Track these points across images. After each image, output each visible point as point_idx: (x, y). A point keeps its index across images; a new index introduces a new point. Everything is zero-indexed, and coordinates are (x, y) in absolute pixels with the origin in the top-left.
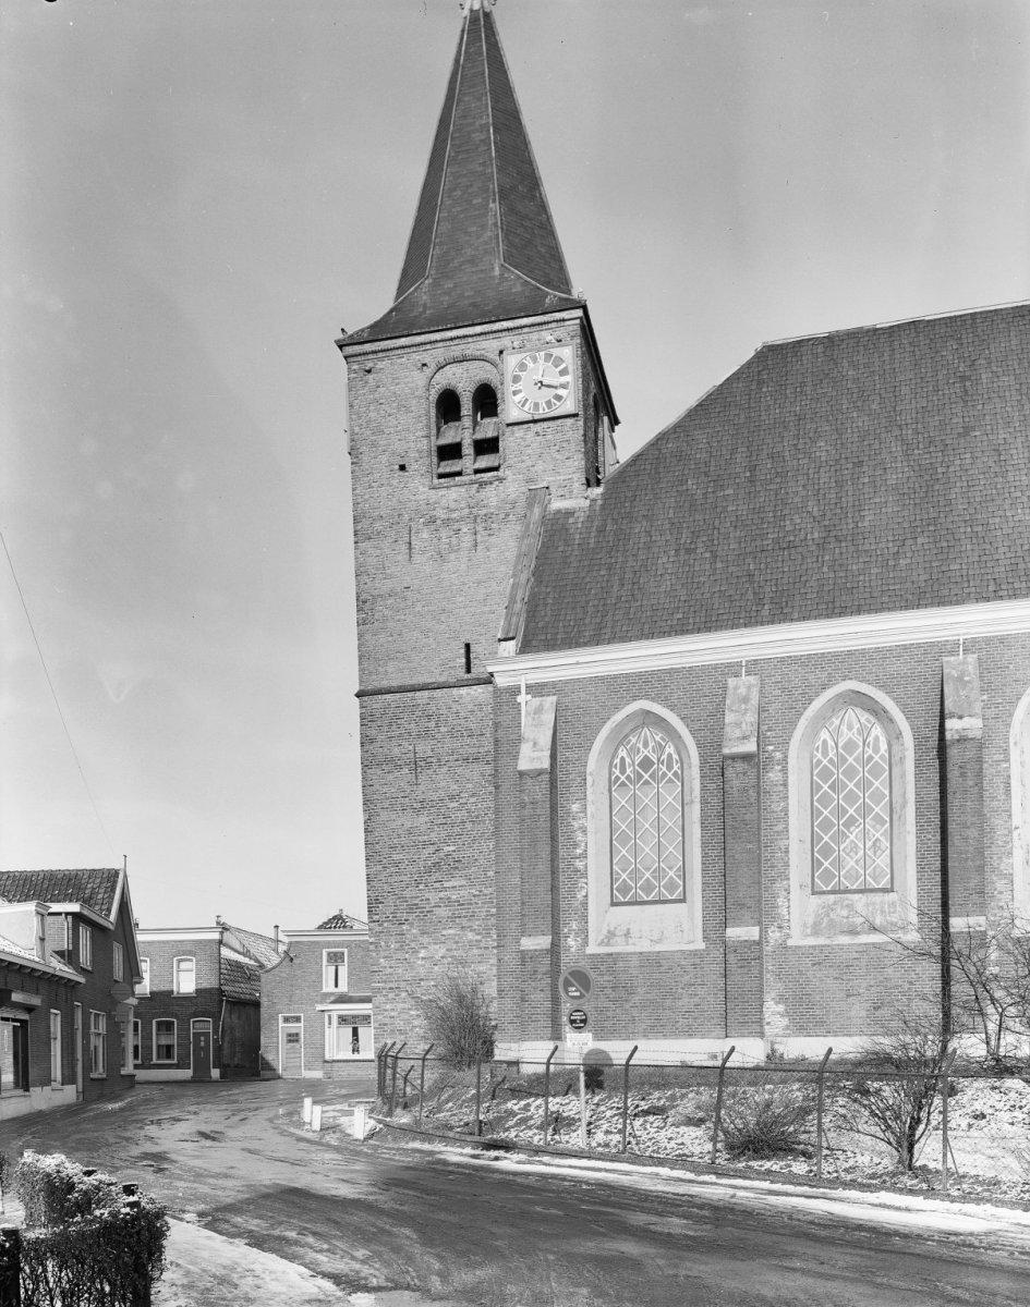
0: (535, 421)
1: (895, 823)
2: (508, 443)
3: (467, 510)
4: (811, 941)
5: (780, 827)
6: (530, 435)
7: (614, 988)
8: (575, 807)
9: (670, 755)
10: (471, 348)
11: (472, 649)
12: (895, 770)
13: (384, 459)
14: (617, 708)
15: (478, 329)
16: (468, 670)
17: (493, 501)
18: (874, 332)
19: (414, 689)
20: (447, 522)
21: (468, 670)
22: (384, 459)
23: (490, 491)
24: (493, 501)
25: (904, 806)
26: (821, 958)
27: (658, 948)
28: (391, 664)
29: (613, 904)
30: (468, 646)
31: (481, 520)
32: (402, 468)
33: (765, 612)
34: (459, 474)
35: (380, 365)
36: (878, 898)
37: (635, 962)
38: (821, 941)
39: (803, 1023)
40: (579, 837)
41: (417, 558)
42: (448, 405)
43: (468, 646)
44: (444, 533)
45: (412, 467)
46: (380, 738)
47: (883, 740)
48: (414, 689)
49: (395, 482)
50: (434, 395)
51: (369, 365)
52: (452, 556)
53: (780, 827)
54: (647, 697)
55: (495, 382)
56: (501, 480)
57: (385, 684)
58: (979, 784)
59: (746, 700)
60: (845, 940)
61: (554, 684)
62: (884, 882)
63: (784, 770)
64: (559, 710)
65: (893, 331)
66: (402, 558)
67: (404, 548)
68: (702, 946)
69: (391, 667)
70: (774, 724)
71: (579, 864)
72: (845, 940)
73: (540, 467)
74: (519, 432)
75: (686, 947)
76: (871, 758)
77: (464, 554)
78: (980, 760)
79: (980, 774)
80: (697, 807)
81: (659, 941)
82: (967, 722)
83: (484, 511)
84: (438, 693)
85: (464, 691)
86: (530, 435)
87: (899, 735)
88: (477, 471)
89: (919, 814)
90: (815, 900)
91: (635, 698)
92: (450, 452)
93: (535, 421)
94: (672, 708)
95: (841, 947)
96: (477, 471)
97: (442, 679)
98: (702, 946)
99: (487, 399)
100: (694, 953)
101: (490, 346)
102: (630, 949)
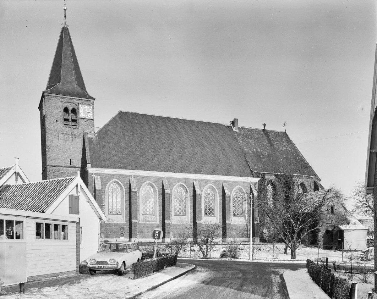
0: (85, 119)
1: (155, 205)
2: (80, 121)
3: (70, 133)
4: (143, 223)
5: (138, 203)
6: (84, 121)
7: (110, 229)
8: (103, 196)
9: (176, 192)
10: (72, 101)
11: (71, 161)
12: (155, 196)
13: (53, 118)
14: (111, 180)
15: (74, 98)
16: (71, 164)
17: (76, 132)
18: (138, 114)
19: (59, 166)
20: (66, 134)
21: (71, 164)
22: (53, 118)
23: (75, 130)
24: (76, 132)
25: (157, 202)
26: (144, 225)
27: (118, 222)
28: (54, 160)
29: (109, 214)
30: (70, 160)
31: (74, 136)
32: (57, 121)
33: (202, 189)
34: (69, 125)
35: (52, 99)
36: (152, 216)
37: (113, 225)
38: (145, 223)
39: (142, 237)
40: (104, 202)
41: (60, 140)
42: (66, 110)
43: (70, 160)
44: (66, 136)
45: (59, 121)
46: (51, 175)
47: (120, 189)
48: (59, 166)
49: (55, 124)
50: (63, 108)
51: (50, 98)
52: (68, 141)
53: (138, 203)
54: (116, 178)
55: (76, 108)
56: (78, 128)
57: (53, 164)
58: (169, 200)
59: (134, 182)
60: (148, 223)
61: (99, 174)
62: (153, 214)
63: (139, 194)
64: (101, 179)
65: (142, 115)
66: (57, 139)
67: (57, 137)
68: (125, 223)
69: (54, 161)
70: (104, 184)
71: (104, 207)
72: (148, 223)
73: (86, 128)
74: (82, 120)
75: (122, 223)
76: (175, 194)
77: (70, 141)
78: (169, 197)
79: (169, 199)
80: (124, 199)
81: (118, 221)
82: (168, 191)
83: (74, 134)
84: (64, 168)
85: (70, 168)
86: (84, 121)
87: (156, 191)
88: (72, 125)
89: (159, 204)
90: (143, 216)
91: (114, 178)
92: (66, 120)
93: (85, 119)
94: (120, 181)
95: (147, 224)
96: (72, 125)
97: (65, 165)
98: (125, 223)
99: (74, 111)
100: (124, 224)
101: (76, 102)
102: (113, 222)
